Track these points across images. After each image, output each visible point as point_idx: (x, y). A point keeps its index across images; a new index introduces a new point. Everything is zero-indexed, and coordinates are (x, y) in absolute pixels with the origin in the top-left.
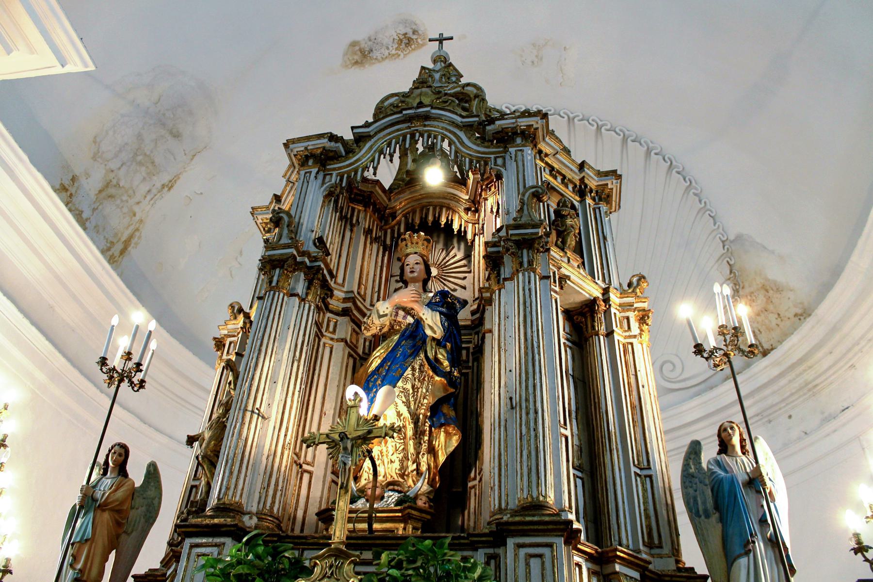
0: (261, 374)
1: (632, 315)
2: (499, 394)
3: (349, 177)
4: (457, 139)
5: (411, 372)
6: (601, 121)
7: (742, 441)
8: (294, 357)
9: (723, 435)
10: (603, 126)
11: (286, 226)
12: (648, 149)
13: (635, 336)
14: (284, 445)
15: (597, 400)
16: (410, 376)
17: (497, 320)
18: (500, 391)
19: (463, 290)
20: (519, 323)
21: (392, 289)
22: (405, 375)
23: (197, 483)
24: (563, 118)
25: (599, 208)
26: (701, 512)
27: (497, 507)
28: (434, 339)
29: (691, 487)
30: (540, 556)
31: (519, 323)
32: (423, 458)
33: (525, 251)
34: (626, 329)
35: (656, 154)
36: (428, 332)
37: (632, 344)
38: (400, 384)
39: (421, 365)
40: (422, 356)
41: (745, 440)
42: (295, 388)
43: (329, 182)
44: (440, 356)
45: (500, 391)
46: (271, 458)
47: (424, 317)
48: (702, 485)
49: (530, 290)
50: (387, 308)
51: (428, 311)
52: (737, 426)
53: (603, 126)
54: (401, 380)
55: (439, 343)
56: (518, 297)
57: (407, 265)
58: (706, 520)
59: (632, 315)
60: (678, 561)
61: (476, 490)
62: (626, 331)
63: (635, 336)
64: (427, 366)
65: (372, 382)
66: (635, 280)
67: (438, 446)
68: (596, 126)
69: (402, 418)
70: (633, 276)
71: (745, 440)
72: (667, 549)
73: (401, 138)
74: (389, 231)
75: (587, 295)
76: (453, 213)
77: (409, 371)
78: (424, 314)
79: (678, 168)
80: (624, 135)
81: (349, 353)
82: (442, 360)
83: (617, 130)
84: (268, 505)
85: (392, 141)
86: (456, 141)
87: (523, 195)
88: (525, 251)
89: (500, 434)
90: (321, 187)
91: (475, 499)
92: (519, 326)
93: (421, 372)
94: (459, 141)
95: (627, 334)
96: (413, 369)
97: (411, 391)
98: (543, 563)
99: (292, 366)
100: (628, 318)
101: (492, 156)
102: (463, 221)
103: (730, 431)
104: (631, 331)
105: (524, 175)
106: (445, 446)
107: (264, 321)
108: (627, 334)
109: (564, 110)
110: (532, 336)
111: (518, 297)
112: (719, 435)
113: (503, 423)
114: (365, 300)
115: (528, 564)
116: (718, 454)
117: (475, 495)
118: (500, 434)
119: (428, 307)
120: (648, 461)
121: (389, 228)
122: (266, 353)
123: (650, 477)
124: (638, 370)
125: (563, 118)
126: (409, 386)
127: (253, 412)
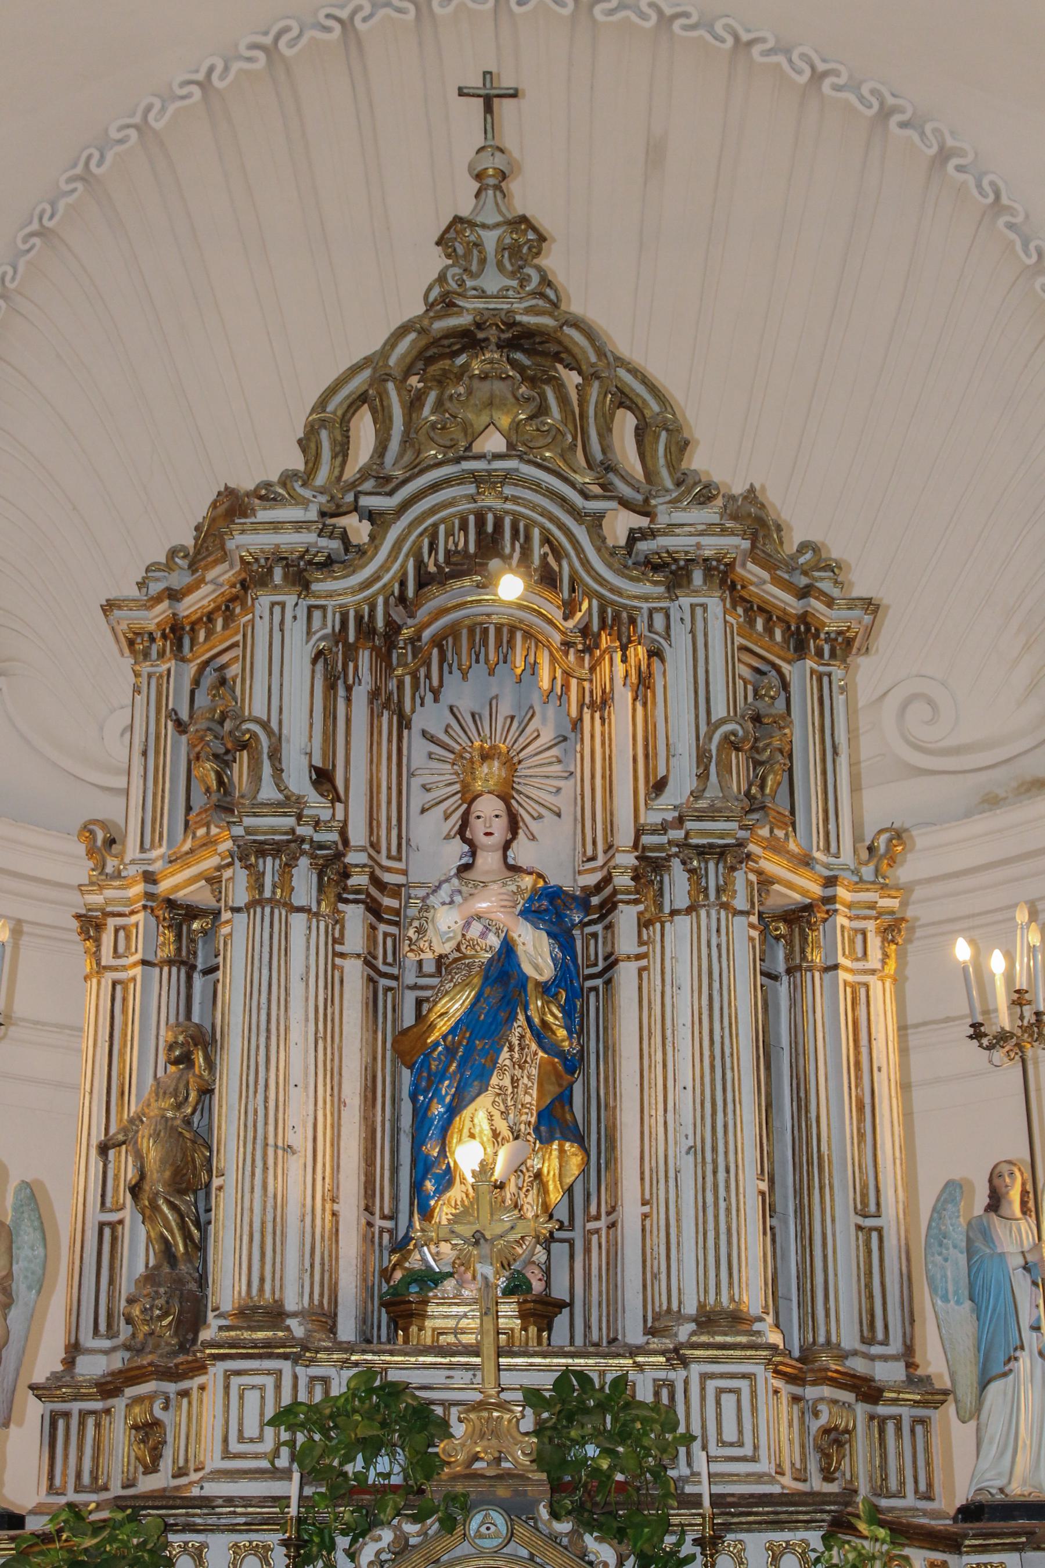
0: (277, 1076)
1: (871, 926)
2: (665, 1123)
3: (359, 618)
4: (575, 549)
5: (507, 1055)
6: (824, 61)
7: (1024, 1193)
8: (316, 1034)
9: (997, 1182)
10: (825, 74)
11: (265, 756)
12: (942, 148)
13: (873, 972)
14: (323, 1196)
15: (802, 1095)
16: (508, 1062)
17: (659, 982)
18: (665, 1117)
19: (556, 818)
20: (700, 1008)
21: (415, 806)
22: (500, 1061)
23: (114, 1217)
24: (723, 41)
25: (829, 675)
26: (950, 1296)
27: (665, 1307)
28: (538, 984)
29: (940, 1254)
30: (737, 1392)
31: (700, 1008)
32: (526, 1196)
33: (711, 865)
34: (860, 955)
35: (960, 169)
36: (528, 969)
37: (867, 986)
38: (494, 1080)
39: (522, 1037)
40: (521, 1017)
41: (1028, 1193)
42: (325, 1091)
43: (322, 629)
44: (550, 1019)
45: (665, 1117)
46: (308, 1219)
47: (519, 941)
48: (956, 1251)
49: (719, 946)
50: (456, 923)
51: (527, 929)
52: (1020, 1170)
53: (825, 74)
54: (495, 1073)
55: (545, 989)
56: (699, 958)
57: (479, 817)
58: (956, 1307)
59: (871, 926)
60: (910, 1365)
61: (600, 1237)
62: (858, 960)
63: (873, 972)
64: (529, 1035)
65: (434, 1059)
66: (882, 842)
67: (548, 1172)
68: (808, 72)
69: (499, 1139)
70: (881, 832)
71: (1028, 1193)
72: (895, 1347)
73: (457, 522)
74: (408, 679)
75: (798, 897)
76: (537, 646)
77: (505, 1054)
78: (520, 936)
79: (1012, 215)
80: (882, 104)
81: (368, 975)
82: (554, 1027)
83: (865, 91)
84: (316, 1297)
85: (437, 528)
86: (572, 553)
87: (710, 737)
88: (711, 865)
89: (667, 1192)
90: (307, 642)
91: (600, 1254)
92: (700, 1014)
93: (522, 1048)
94: (578, 556)
95: (859, 965)
96: (511, 1049)
97: (510, 1090)
98: (739, 1401)
99: (316, 1051)
100: (864, 933)
101: (645, 606)
102: (559, 673)
103: (1008, 1180)
104: (867, 961)
105: (707, 672)
106: (560, 1174)
107: (265, 972)
108: (859, 965)
109: (725, 20)
110: (722, 1037)
111: (699, 958)
112: (990, 1181)
113: (672, 1174)
114: (379, 852)
115: (718, 1403)
116: (986, 1210)
117: (600, 1247)
118: (667, 1192)
119: (526, 919)
120: (878, 1204)
121: (409, 673)
122: (278, 1036)
123: (879, 1230)
124: (873, 1038)
125: (723, 41)
126: (507, 1082)
127: (276, 1146)
